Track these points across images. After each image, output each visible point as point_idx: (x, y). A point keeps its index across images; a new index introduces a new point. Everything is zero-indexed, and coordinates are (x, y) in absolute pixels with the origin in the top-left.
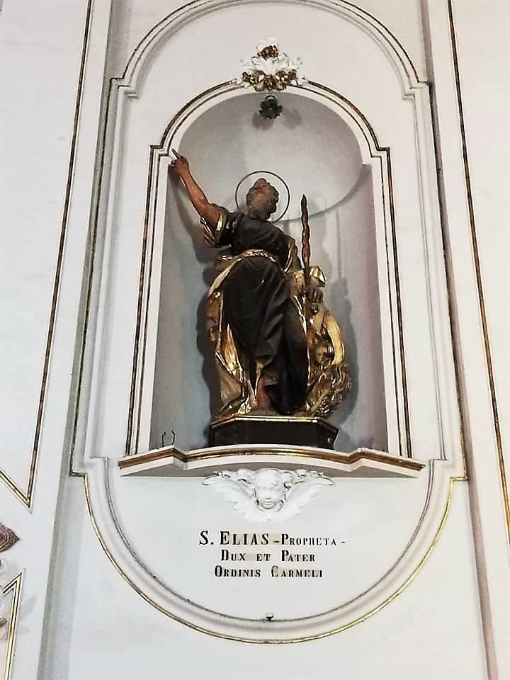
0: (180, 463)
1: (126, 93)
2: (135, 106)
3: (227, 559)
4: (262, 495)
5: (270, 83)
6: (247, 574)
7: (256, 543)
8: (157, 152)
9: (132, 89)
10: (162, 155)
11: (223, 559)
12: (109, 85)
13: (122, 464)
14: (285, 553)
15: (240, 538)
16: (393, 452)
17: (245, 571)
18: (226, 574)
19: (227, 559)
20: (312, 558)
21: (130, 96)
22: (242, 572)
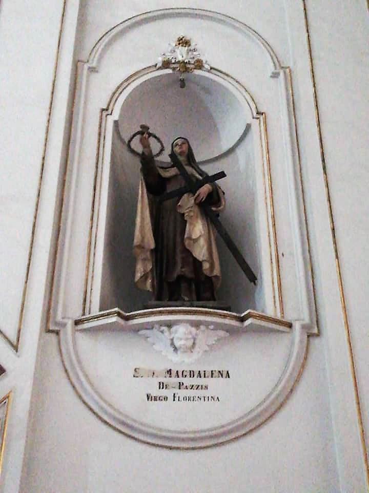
0: (122, 322)
1: (89, 68)
2: (95, 78)
3: (163, 388)
4: (178, 343)
5: (184, 67)
6: (214, 399)
7: (178, 377)
8: (105, 113)
9: (94, 65)
10: (108, 115)
11: (160, 388)
12: (77, 65)
13: (77, 323)
14: (181, 384)
15: (208, 374)
16: (270, 311)
17: (212, 397)
18: (155, 400)
19: (163, 388)
20: (206, 387)
21: (92, 70)
22: (210, 398)
